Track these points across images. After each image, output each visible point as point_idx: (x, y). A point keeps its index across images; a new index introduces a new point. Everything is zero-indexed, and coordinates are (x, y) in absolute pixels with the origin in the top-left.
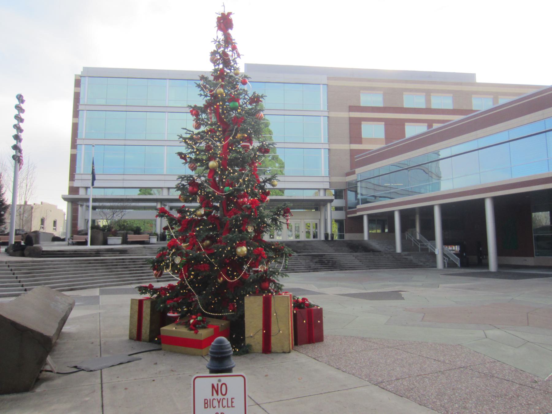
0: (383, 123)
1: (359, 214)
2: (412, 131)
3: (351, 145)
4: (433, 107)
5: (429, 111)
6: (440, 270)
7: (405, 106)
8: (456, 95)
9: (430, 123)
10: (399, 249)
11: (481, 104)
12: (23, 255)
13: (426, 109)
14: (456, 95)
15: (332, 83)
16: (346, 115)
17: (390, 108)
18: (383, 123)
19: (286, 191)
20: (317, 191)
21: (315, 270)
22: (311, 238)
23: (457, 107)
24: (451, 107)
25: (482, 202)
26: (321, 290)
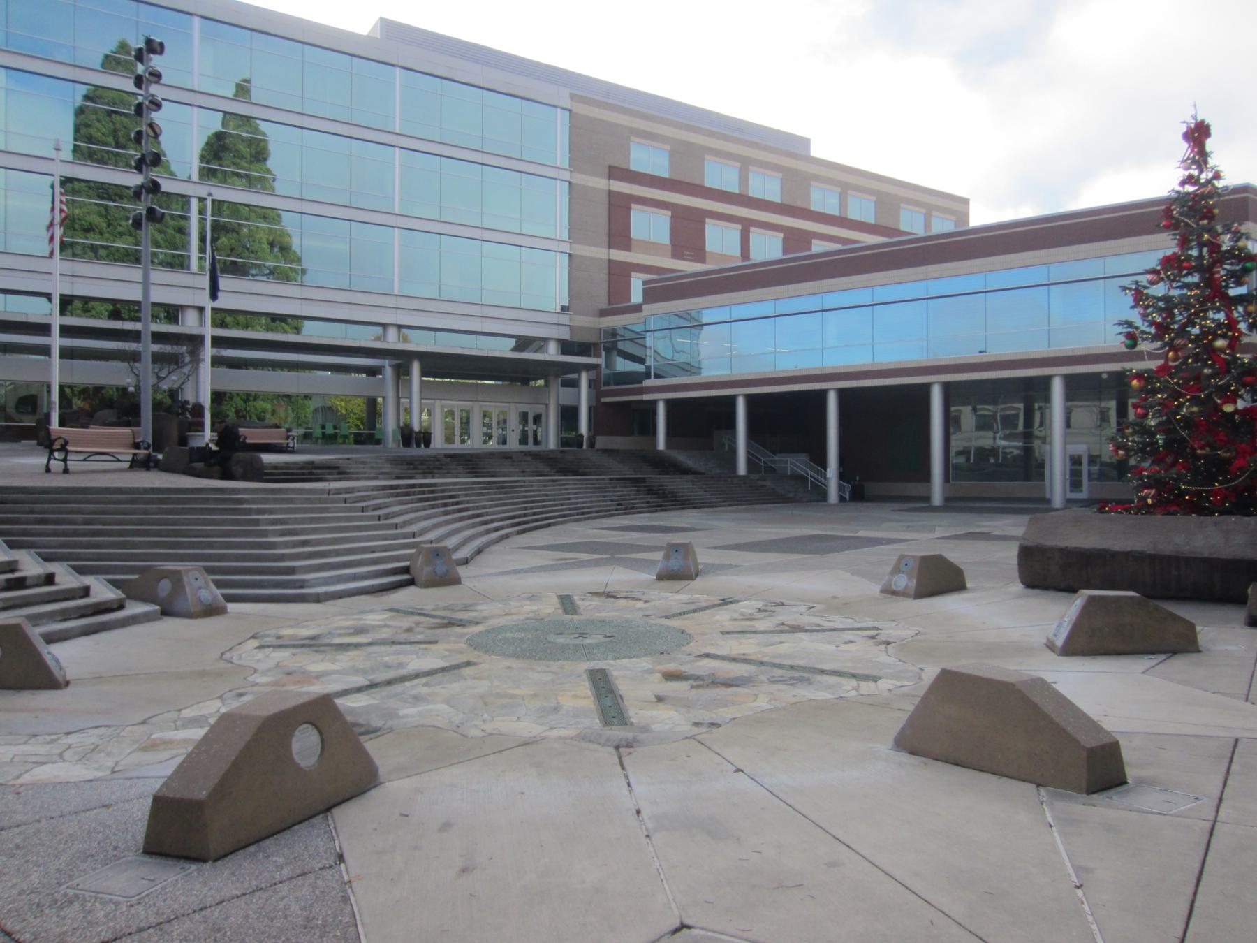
0: (669, 213)
1: (646, 397)
2: (721, 241)
3: (575, 246)
4: (753, 193)
5: (743, 200)
6: (834, 505)
7: (707, 184)
8: (681, 152)
10: (742, 469)
11: (912, 224)
12: (226, 476)
13: (874, 225)
15: (580, 109)
16: (601, 183)
17: (681, 182)
18: (669, 213)
19: (307, 325)
20: (379, 330)
21: (629, 509)
22: (530, 447)
24: (777, 199)
26: (907, 536)
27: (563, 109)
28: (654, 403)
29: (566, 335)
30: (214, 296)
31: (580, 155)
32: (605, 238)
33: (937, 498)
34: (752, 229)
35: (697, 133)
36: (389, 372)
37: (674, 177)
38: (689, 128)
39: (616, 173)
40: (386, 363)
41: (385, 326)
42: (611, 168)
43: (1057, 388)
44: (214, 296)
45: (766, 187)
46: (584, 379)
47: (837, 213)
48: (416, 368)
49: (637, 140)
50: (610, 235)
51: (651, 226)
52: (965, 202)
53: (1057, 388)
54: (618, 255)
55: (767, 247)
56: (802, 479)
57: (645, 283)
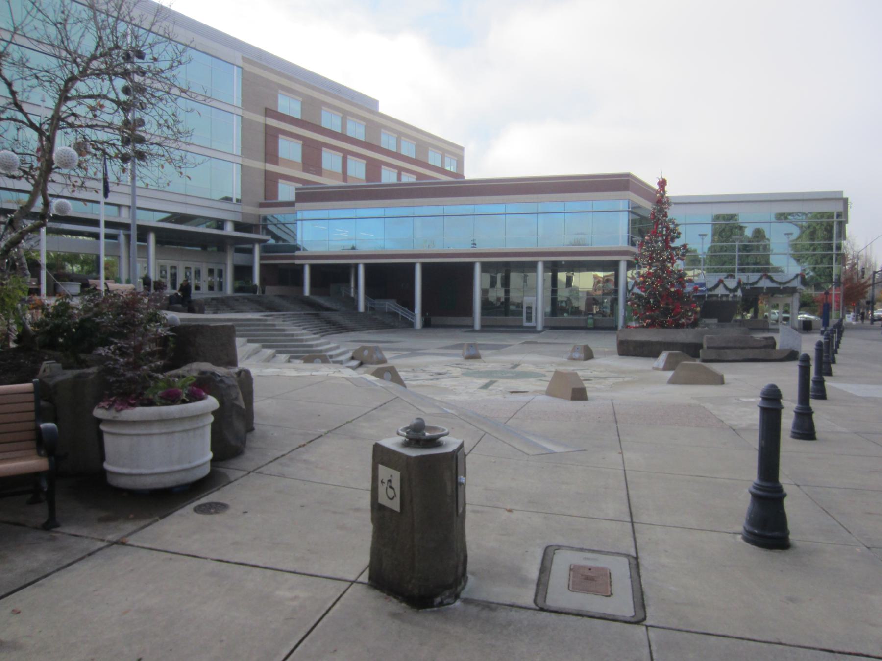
1: (297, 262)
2: (388, 177)
4: (350, 133)
8: (309, 104)
9: (420, 176)
10: (361, 308)
13: (341, 134)
14: (309, 104)
16: (260, 119)
17: (309, 123)
18: (301, 142)
23: (368, 141)
24: (298, 116)
25: (412, 266)
27: (238, 66)
28: (302, 267)
29: (239, 219)
30: (106, 195)
31: (248, 101)
32: (263, 155)
33: (477, 326)
34: (349, 157)
35: (320, 92)
36: (122, 239)
37: (367, 141)
38: (314, 88)
39: (270, 112)
40: (122, 233)
41: (119, 206)
42: (266, 109)
43: (540, 267)
44: (106, 195)
45: (356, 130)
46: (257, 249)
47: (394, 150)
48: (152, 238)
49: (283, 92)
50: (266, 154)
51: (290, 150)
52: (462, 149)
53: (540, 267)
54: (271, 167)
55: (357, 171)
56: (395, 315)
57: (297, 189)
